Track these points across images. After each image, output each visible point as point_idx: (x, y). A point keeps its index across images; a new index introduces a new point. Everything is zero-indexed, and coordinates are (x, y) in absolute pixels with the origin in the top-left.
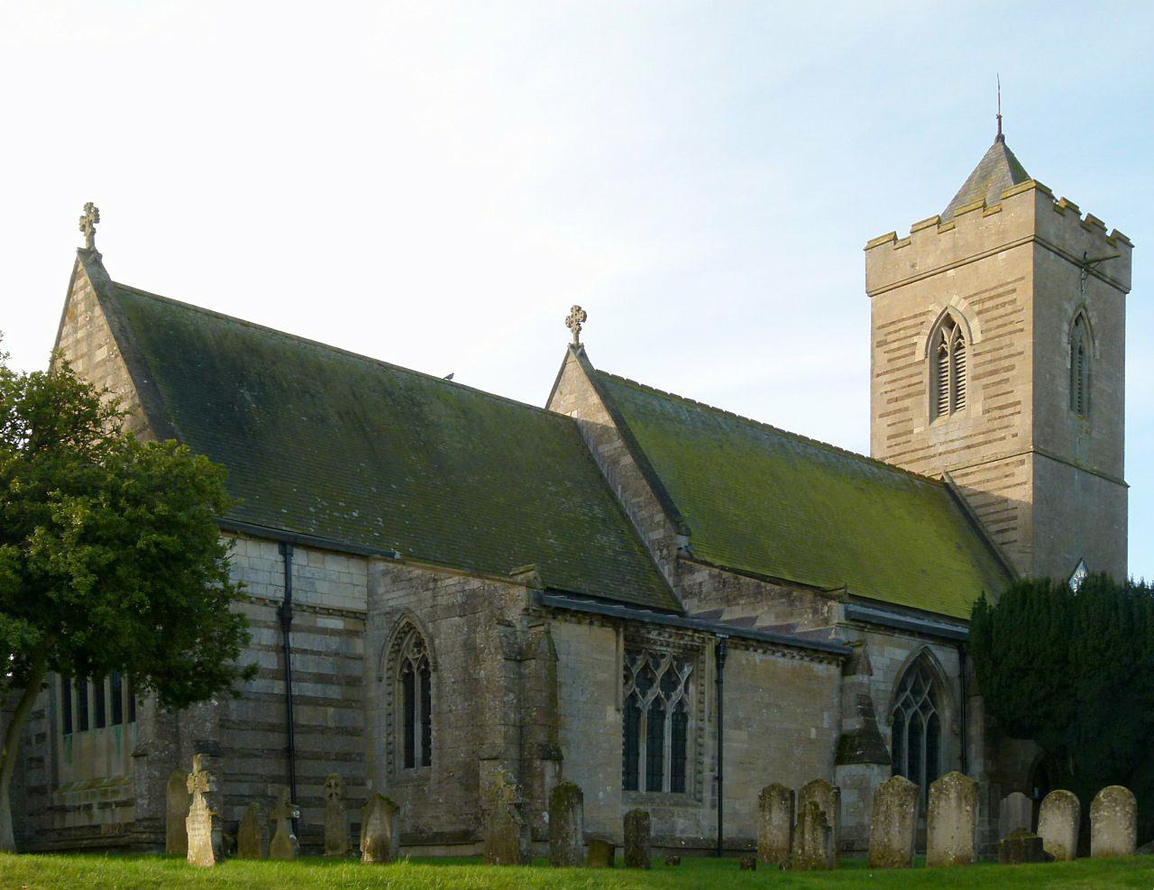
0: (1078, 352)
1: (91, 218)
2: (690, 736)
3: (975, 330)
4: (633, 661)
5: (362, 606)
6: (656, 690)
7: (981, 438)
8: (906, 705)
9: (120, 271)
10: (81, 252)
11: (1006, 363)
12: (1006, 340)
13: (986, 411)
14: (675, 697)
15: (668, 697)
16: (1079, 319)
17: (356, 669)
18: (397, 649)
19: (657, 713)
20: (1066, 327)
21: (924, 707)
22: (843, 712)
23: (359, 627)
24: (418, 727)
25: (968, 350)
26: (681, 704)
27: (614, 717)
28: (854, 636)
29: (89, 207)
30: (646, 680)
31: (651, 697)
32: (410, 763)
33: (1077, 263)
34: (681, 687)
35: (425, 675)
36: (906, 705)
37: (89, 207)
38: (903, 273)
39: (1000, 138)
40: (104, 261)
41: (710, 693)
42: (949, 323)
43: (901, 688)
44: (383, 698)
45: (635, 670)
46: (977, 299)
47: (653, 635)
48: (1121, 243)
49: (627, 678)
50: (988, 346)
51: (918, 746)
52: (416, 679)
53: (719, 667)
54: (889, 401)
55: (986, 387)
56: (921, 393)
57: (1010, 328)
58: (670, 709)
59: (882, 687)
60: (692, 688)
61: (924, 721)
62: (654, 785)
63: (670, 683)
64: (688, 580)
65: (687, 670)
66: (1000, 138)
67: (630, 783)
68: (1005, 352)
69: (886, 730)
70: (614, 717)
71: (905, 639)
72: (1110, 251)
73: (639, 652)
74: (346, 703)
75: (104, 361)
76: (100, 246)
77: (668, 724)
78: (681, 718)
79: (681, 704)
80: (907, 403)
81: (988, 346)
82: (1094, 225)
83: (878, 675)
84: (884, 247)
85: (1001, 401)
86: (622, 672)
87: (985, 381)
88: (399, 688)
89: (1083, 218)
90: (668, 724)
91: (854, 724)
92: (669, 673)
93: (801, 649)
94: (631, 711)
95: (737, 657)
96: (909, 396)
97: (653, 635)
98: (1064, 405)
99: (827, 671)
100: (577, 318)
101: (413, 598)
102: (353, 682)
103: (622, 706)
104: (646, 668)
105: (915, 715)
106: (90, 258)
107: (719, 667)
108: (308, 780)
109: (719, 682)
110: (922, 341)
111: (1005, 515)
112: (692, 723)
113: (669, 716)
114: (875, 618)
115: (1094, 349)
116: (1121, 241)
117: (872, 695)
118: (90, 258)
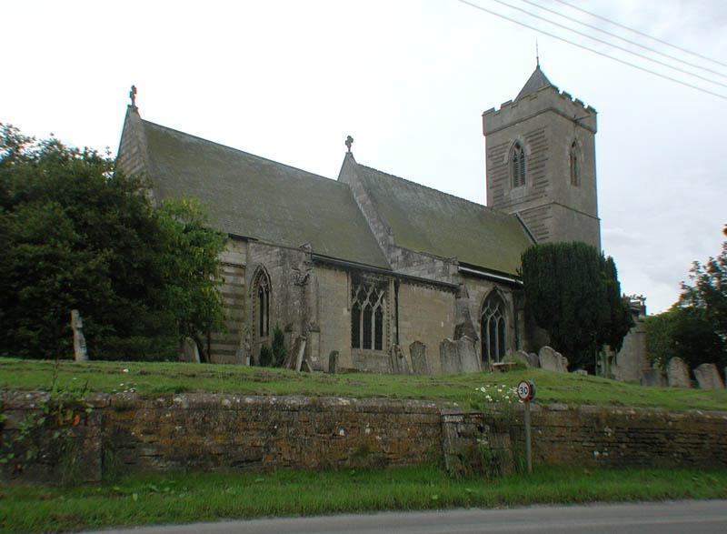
0: (574, 159)
1: (349, 141)
2: (384, 324)
3: (528, 151)
4: (356, 288)
5: (243, 263)
6: (367, 302)
7: (532, 197)
8: (488, 313)
9: (147, 114)
10: (129, 106)
11: (542, 163)
12: (540, 154)
13: (533, 185)
14: (376, 306)
15: (373, 305)
16: (574, 145)
17: (240, 291)
18: (257, 282)
19: (368, 311)
20: (567, 148)
21: (496, 314)
22: (457, 316)
23: (242, 271)
24: (265, 317)
25: (526, 159)
26: (379, 308)
27: (346, 313)
28: (460, 280)
29: (349, 137)
30: (362, 297)
31: (376, 306)
32: (262, 335)
33: (571, 120)
34: (379, 301)
35: (267, 293)
36: (488, 313)
37: (349, 137)
38: (499, 125)
39: (538, 67)
40: (139, 111)
41: (392, 306)
42: (518, 146)
43: (485, 305)
44: (251, 303)
45: (357, 292)
46: (528, 136)
47: (365, 276)
48: (591, 112)
49: (353, 295)
50: (533, 156)
51: (494, 332)
52: (263, 294)
53: (396, 291)
54: (494, 181)
55: (534, 174)
56: (507, 177)
57: (542, 148)
58: (374, 309)
59: (475, 304)
60: (384, 301)
61: (497, 321)
62: (367, 346)
63: (374, 298)
64: (392, 255)
65: (382, 293)
66: (538, 67)
67: (355, 344)
68: (541, 159)
69: (477, 324)
70: (346, 313)
71: (486, 282)
72: (586, 115)
73: (358, 284)
74: (235, 307)
75: (136, 153)
76: (136, 105)
77: (373, 318)
78: (379, 314)
79: (379, 308)
80: (500, 182)
81: (533, 156)
82: (579, 103)
83: (472, 298)
84: (489, 115)
85: (540, 180)
86: (350, 292)
87: (534, 171)
88: (258, 299)
89: (574, 100)
90: (373, 318)
91: (462, 320)
92: (373, 293)
93: (421, 282)
94: (355, 311)
95: (402, 288)
96: (501, 179)
97: (365, 276)
98: (569, 182)
99: (451, 296)
100: (349, 141)
101: (263, 258)
102: (238, 297)
103: (350, 308)
104: (362, 291)
105: (492, 318)
106: (133, 109)
107: (396, 291)
108: (217, 342)
109: (396, 299)
110: (506, 154)
111: (544, 231)
112: (385, 317)
113: (374, 314)
114: (470, 274)
115: (581, 158)
116: (591, 111)
117: (470, 307)
118: (133, 109)
